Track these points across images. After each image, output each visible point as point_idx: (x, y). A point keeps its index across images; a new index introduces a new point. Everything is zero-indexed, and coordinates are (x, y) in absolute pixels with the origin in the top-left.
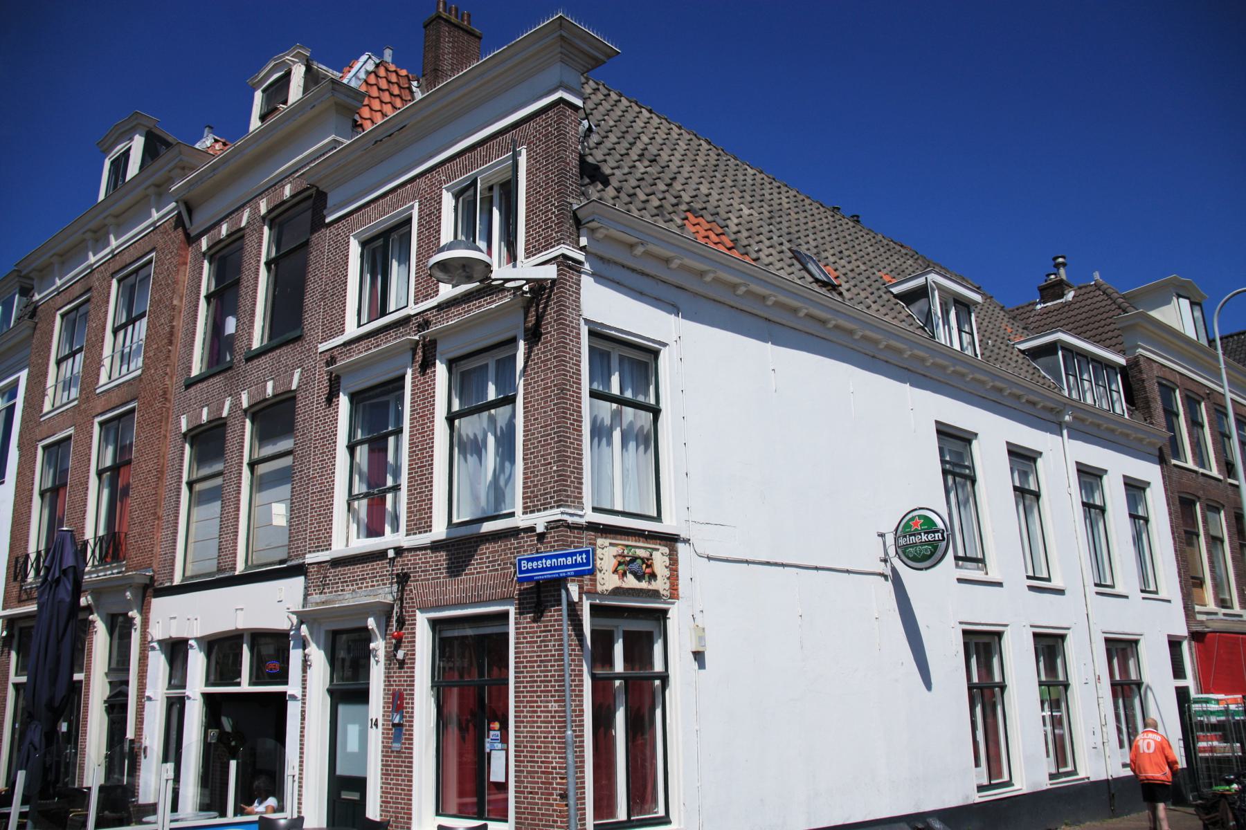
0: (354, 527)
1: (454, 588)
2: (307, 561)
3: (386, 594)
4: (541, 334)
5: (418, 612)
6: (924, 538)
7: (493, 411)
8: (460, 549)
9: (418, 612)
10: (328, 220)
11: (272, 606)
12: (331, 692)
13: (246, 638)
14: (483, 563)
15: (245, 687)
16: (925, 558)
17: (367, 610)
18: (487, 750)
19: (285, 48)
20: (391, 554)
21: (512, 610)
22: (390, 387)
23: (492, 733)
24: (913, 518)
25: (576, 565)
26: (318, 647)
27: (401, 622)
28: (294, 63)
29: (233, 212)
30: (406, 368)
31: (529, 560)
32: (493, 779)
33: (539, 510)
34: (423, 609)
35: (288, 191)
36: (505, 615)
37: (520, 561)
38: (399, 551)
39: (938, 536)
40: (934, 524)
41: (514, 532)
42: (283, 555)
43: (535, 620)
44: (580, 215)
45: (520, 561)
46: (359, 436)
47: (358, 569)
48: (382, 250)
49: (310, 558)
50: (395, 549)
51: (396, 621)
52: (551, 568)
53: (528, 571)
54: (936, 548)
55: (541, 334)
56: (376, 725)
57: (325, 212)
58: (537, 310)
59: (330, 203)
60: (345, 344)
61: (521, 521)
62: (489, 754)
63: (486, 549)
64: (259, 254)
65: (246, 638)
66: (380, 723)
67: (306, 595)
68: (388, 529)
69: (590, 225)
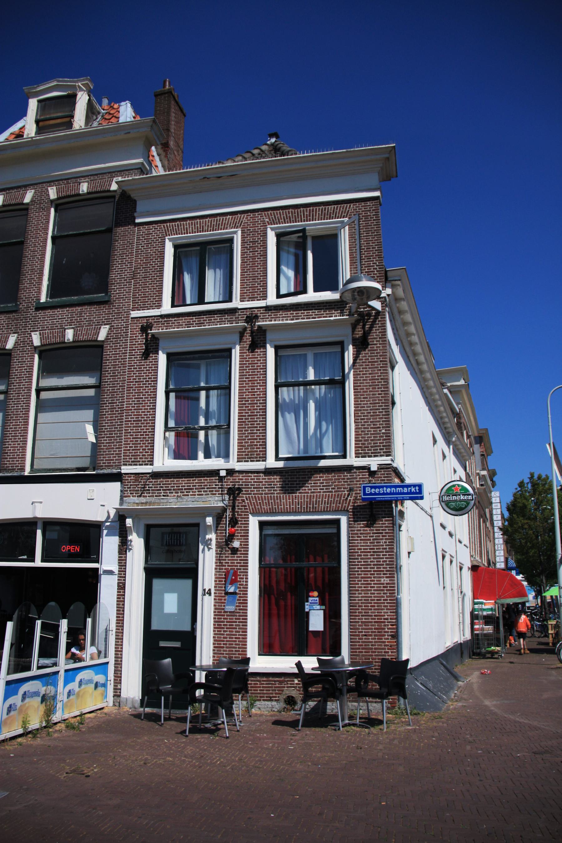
0: (166, 450)
1: (287, 500)
2: (123, 471)
3: (216, 501)
4: (369, 344)
5: (250, 516)
6: (462, 497)
7: (313, 387)
8: (295, 476)
9: (250, 516)
10: (138, 221)
11: (93, 502)
12: (146, 569)
13: (40, 525)
14: (314, 488)
15: (38, 563)
16: (461, 509)
17: (205, 512)
18: (307, 610)
19: (77, 75)
20: (223, 473)
21: (344, 520)
22: (210, 355)
23: (310, 599)
24: (454, 486)
25: (411, 493)
26: (139, 536)
27: (234, 522)
28: (81, 90)
29: (12, 188)
30: (235, 344)
31: (372, 487)
32: (311, 628)
33: (370, 456)
34: (254, 514)
35: (84, 188)
36: (337, 522)
37: (364, 487)
38: (230, 472)
39: (470, 497)
40: (468, 490)
41: (349, 469)
42: (86, 463)
43: (367, 526)
44: (389, 274)
45: (364, 487)
46: (171, 387)
47: (183, 482)
48: (198, 256)
49: (125, 469)
50: (227, 470)
51: (230, 522)
52: (391, 494)
53: (371, 494)
54: (468, 504)
55: (369, 344)
56: (210, 594)
57: (135, 214)
58: (363, 327)
59: (139, 208)
60: (162, 316)
61: (352, 460)
62: (308, 613)
63: (320, 478)
64: (47, 229)
65: (40, 525)
66: (213, 591)
67: (122, 498)
68: (201, 455)
69: (394, 282)
